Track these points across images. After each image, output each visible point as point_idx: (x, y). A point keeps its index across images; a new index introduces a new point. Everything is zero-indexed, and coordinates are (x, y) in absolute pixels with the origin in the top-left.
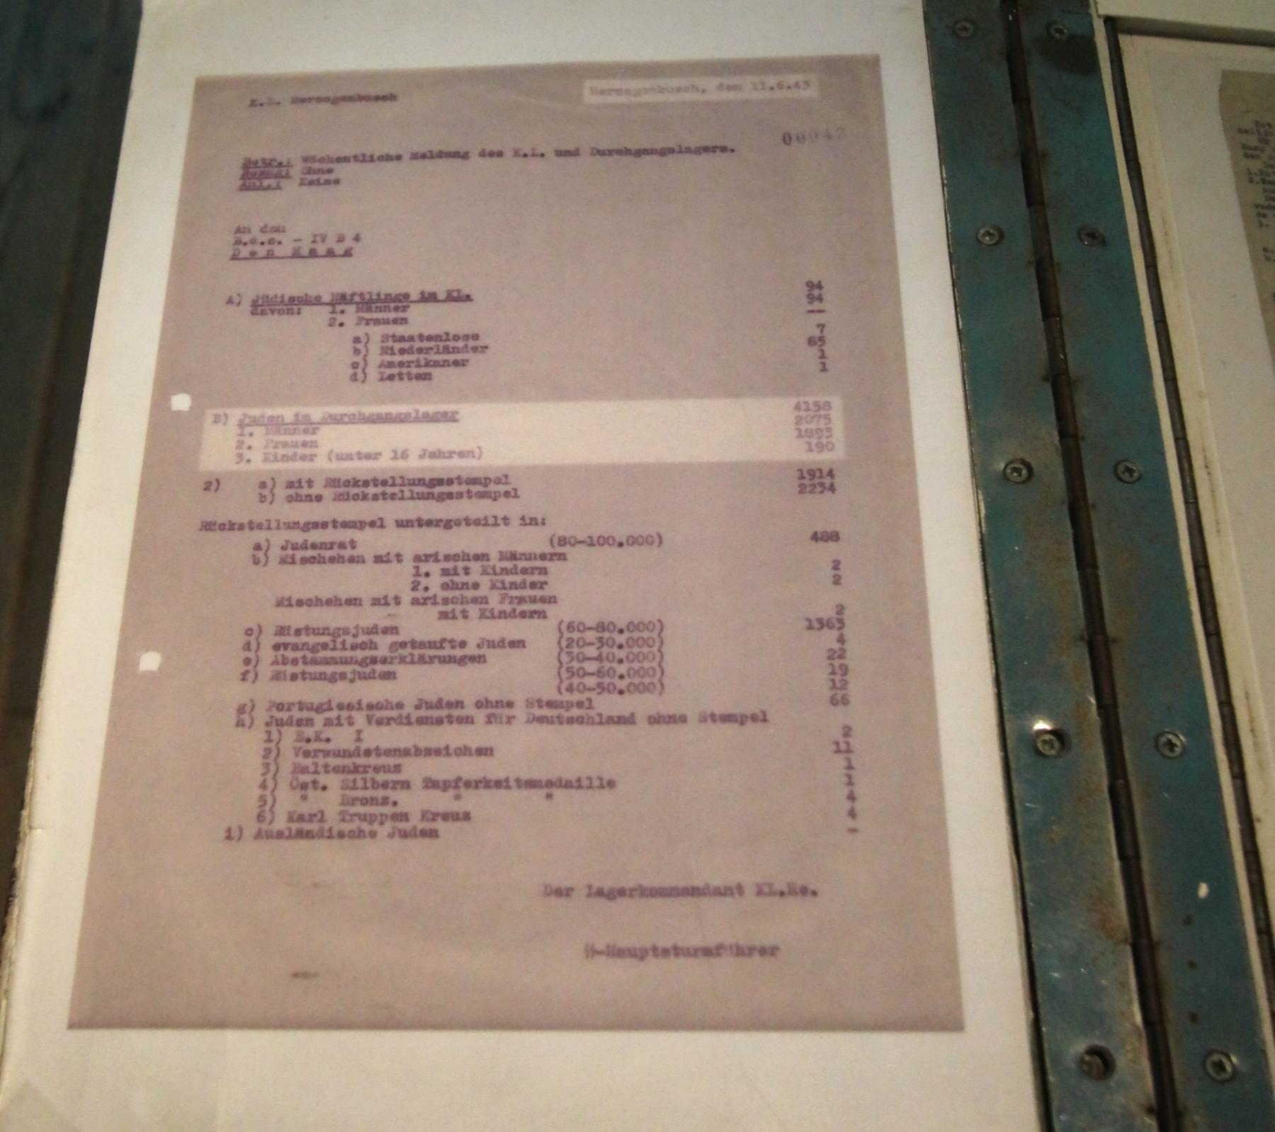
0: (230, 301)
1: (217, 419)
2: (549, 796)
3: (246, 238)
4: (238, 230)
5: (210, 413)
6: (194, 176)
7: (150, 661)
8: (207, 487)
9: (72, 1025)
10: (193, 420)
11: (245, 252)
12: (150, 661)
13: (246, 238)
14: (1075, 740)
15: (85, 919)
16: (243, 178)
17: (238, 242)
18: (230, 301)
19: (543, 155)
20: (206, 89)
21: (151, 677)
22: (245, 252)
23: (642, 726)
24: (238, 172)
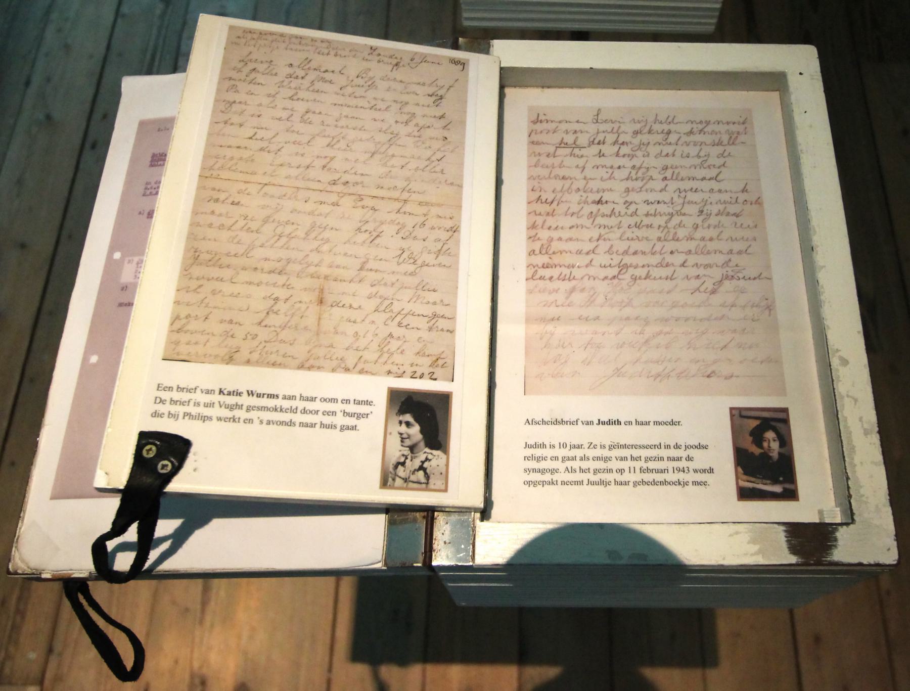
0: (140, 213)
1: (129, 262)
2: (32, 381)
3: (149, 187)
4: (147, 184)
5: (127, 259)
6: (134, 161)
7: (94, 359)
8: (122, 289)
9: (52, 499)
10: (119, 264)
11: (148, 192)
12: (94, 359)
13: (149, 187)
14: (817, 229)
15: (61, 459)
16: (151, 161)
17: (146, 188)
18: (140, 213)
19: (347, 349)
20: (142, 124)
21: (94, 365)
22: (148, 192)
23: (243, 389)
24: (150, 159)
